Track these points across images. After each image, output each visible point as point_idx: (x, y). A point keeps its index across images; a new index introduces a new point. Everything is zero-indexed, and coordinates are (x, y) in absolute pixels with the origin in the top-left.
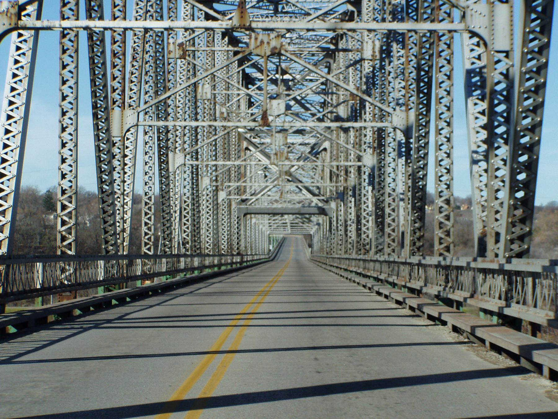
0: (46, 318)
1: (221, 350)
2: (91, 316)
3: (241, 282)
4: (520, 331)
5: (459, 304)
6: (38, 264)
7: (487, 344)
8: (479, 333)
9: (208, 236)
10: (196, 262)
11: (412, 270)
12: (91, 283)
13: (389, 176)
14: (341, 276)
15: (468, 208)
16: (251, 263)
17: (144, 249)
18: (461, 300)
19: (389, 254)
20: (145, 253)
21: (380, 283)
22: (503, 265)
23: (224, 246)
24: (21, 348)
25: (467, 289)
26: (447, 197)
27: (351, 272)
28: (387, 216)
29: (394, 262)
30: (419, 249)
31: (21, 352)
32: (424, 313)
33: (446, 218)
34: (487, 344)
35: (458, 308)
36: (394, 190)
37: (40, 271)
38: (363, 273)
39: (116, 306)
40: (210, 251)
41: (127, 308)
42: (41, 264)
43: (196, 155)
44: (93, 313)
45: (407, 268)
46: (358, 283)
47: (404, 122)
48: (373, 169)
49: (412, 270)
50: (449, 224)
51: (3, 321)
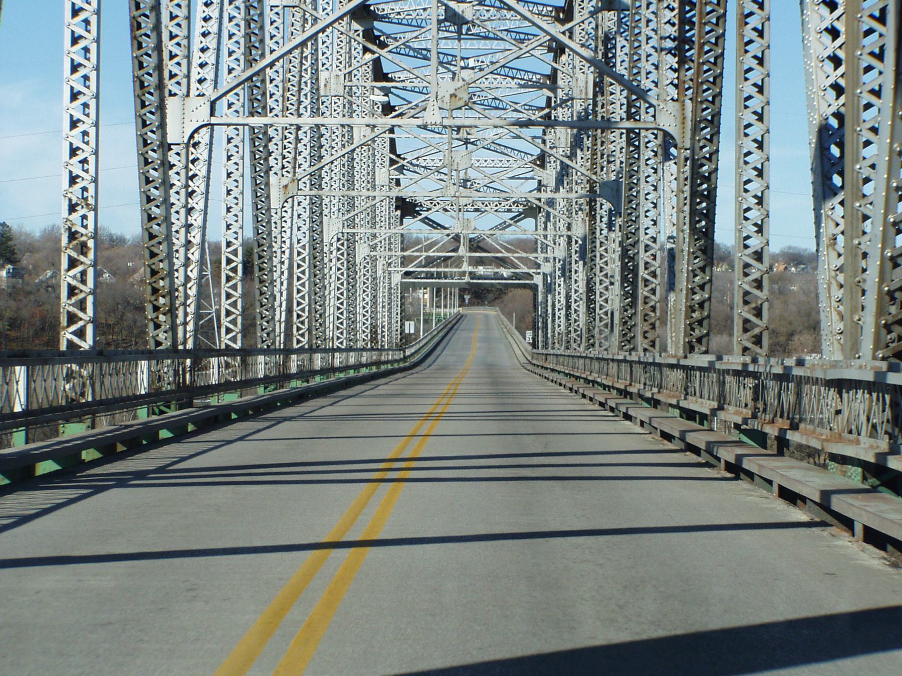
0: (32, 468)
1: (401, 457)
2: (115, 464)
3: (414, 384)
4: (783, 456)
5: (703, 417)
6: (17, 368)
7: (858, 528)
8: (838, 504)
9: (338, 318)
10: (318, 361)
11: (688, 378)
12: (129, 398)
13: (646, 216)
14: (545, 378)
15: (786, 268)
16: (342, 375)
17: (67, 335)
18: (707, 412)
19: (645, 350)
20: (227, 345)
21: (628, 400)
22: (790, 368)
23: (363, 337)
24: (63, 495)
25: (786, 415)
26: (758, 248)
27: (559, 372)
28: (641, 284)
29: (654, 364)
30: (699, 340)
31: (46, 506)
32: (719, 459)
33: (755, 285)
34: (858, 528)
35: (701, 423)
36: (654, 240)
37: (145, 371)
38: (599, 380)
39: (167, 441)
40: (234, 339)
41: (136, 462)
42: (24, 368)
43: (351, 222)
44: (122, 456)
45: (679, 374)
46: (591, 399)
47: (583, 232)
48: (584, 239)
49: (688, 378)
50: (762, 295)
51: (54, 450)
